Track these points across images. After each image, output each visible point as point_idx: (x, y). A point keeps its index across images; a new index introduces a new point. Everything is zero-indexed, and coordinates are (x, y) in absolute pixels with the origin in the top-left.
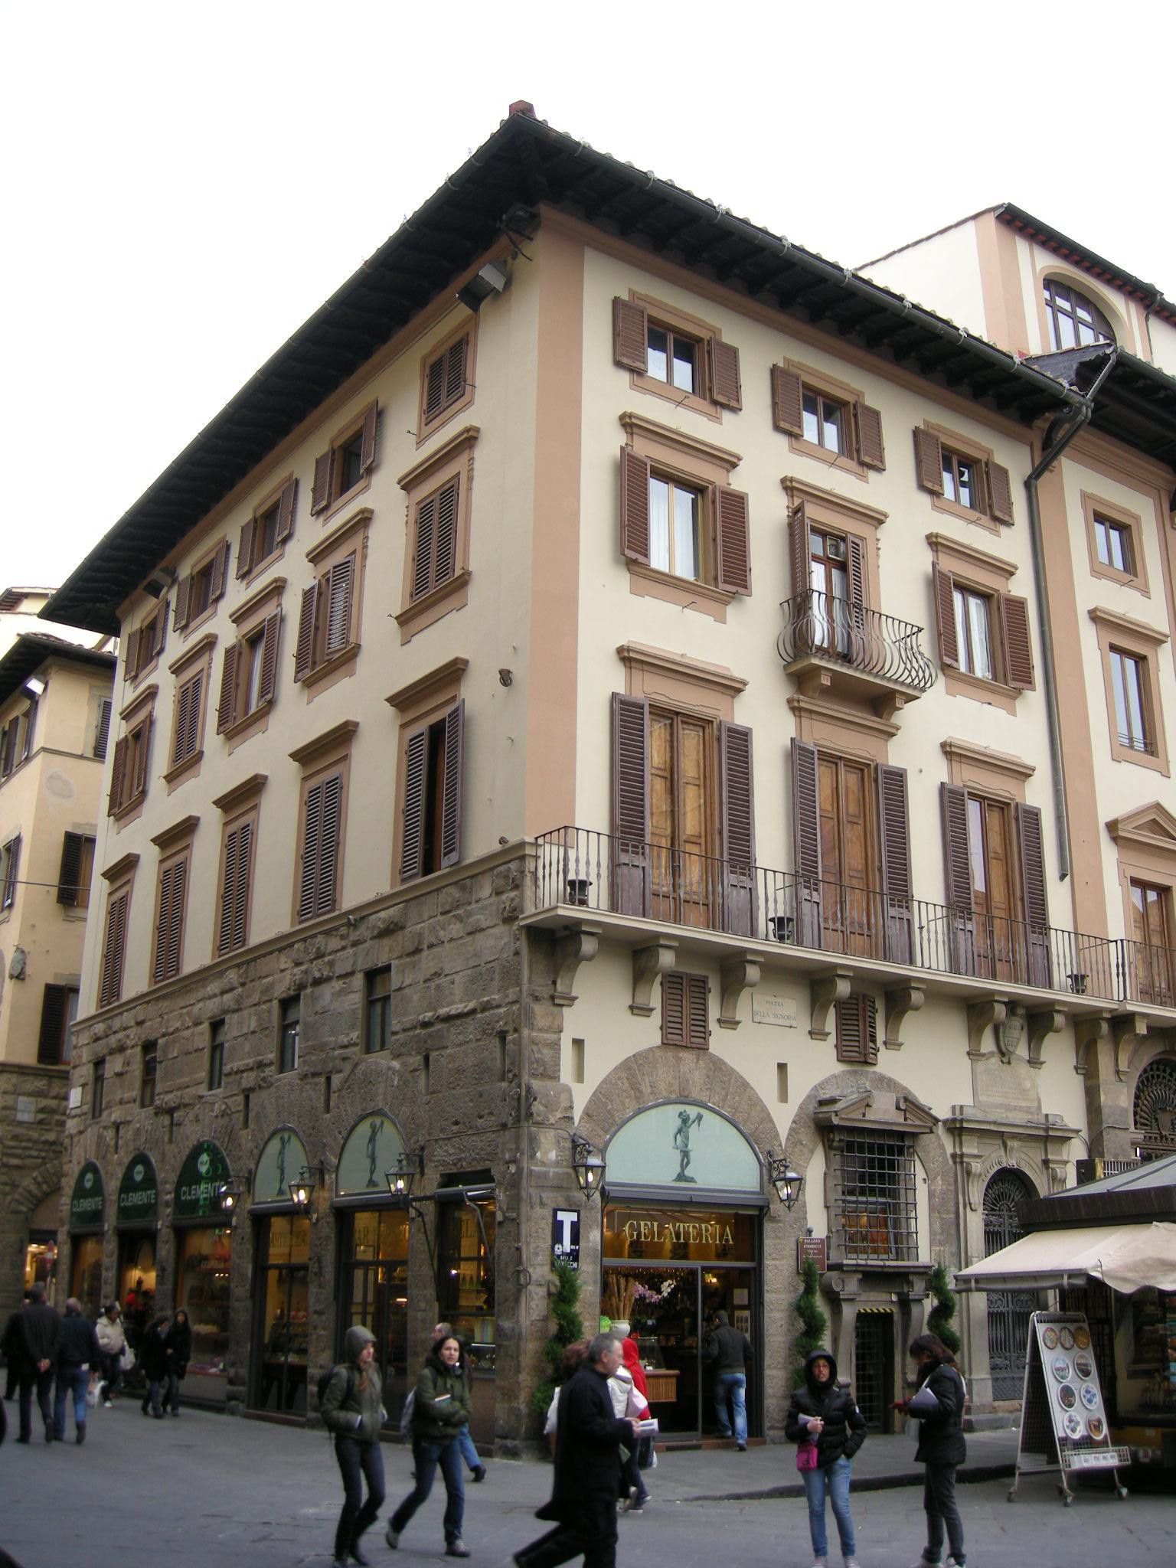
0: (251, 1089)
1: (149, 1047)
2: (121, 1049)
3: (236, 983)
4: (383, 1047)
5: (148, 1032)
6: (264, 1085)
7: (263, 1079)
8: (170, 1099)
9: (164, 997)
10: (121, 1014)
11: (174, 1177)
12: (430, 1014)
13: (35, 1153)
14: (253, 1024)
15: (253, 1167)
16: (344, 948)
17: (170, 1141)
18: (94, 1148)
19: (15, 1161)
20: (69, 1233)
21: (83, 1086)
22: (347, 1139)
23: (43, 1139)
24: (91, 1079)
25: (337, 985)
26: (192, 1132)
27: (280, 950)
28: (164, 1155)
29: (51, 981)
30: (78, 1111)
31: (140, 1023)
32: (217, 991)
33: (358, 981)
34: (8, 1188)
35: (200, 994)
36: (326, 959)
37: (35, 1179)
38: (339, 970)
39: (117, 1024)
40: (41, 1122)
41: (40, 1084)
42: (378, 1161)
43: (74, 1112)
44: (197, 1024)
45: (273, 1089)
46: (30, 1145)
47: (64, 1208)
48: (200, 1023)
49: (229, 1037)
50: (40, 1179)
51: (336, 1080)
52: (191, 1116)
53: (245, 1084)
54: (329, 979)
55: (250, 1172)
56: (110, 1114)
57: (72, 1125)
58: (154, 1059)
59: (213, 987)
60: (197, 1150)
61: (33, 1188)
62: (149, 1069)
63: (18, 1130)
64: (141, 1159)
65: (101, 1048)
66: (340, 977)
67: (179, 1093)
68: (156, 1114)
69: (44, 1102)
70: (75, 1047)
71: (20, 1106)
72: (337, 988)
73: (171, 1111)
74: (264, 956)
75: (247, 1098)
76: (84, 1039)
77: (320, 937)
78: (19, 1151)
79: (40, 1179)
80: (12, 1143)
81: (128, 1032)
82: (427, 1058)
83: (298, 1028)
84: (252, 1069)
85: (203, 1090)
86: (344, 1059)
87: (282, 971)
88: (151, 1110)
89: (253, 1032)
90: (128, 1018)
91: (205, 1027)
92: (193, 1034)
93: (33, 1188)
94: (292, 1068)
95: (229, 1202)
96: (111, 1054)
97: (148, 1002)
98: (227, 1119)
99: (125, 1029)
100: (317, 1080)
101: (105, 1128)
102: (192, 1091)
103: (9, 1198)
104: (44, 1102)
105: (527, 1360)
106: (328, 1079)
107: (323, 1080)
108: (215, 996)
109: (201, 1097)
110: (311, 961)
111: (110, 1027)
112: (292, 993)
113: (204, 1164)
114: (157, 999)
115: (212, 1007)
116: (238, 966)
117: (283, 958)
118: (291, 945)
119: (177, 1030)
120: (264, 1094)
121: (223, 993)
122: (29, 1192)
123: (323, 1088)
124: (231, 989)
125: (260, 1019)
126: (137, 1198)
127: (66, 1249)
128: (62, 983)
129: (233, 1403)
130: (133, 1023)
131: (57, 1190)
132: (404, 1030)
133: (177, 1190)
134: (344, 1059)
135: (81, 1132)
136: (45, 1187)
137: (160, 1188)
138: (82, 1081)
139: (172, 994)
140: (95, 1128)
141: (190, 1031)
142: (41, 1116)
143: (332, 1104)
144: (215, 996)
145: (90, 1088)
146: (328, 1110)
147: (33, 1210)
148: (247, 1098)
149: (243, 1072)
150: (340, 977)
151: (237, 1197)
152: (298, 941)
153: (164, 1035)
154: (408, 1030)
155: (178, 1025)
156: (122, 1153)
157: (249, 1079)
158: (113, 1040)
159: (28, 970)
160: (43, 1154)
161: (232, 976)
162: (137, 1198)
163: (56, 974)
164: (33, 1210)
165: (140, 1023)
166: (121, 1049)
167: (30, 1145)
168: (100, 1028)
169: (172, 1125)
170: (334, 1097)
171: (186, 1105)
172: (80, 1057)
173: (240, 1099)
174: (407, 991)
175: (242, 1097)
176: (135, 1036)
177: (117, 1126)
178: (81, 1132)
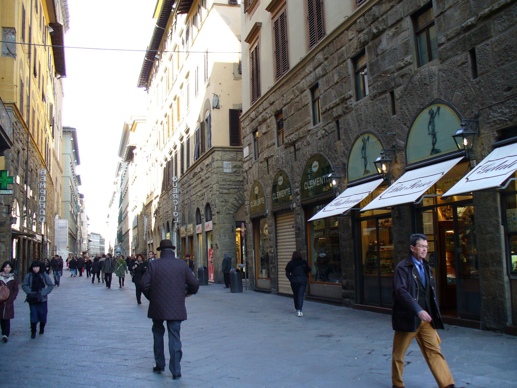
0: (340, 116)
1: (278, 114)
2: (264, 120)
3: (322, 60)
4: (431, 59)
5: (277, 106)
6: (347, 110)
7: (347, 108)
8: (293, 137)
9: (283, 85)
10: (262, 103)
11: (298, 179)
12: (472, 19)
13: (234, 187)
14: (336, 78)
15: (345, 161)
16: (392, 7)
17: (296, 160)
18: (257, 174)
19: (225, 191)
20: (250, 218)
21: (249, 145)
22: (410, 128)
23: (237, 180)
24: (252, 141)
25: (390, 32)
26: (307, 151)
27: (347, 29)
28: (292, 168)
29: (232, 108)
30: (248, 158)
31: (271, 104)
32: (312, 69)
33: (408, 23)
34: (224, 203)
35: (303, 74)
36: (380, 19)
37: (235, 198)
38: (390, 22)
39: (261, 109)
40: (235, 172)
41: (233, 154)
42: (438, 135)
43: (246, 159)
44: (302, 92)
45: (353, 112)
46: (231, 183)
47: (247, 206)
48: (305, 90)
49: (322, 92)
50: (237, 198)
51: (398, 92)
52: (305, 143)
53: (335, 115)
54: (384, 31)
55: (344, 165)
56: (263, 155)
57: (246, 166)
58: (282, 120)
59: (309, 68)
60: (313, 158)
61: (235, 202)
62: (280, 126)
63: (225, 177)
64: (281, 172)
65: (254, 124)
66: (392, 26)
67: (297, 133)
68: (286, 148)
69: (235, 163)
70: (243, 128)
71: (225, 166)
72: (391, 34)
73: (293, 144)
74: (338, 37)
75: (337, 122)
76: (246, 122)
77: (374, 8)
78: (227, 186)
79: (237, 198)
80: (223, 183)
81: (267, 110)
82: (473, 52)
83: (366, 70)
84: (338, 104)
85: (311, 127)
86: (402, 76)
87: (350, 40)
88: (283, 146)
89: (337, 83)
90: (266, 104)
91: (308, 92)
92: (301, 99)
93: (235, 202)
94: (365, 95)
95: (334, 182)
96: (260, 125)
97: (275, 92)
98: (326, 138)
99: (265, 110)
100: (383, 96)
101: (261, 162)
102: (305, 129)
103: (225, 208)
104: (235, 163)
105: (345, 291)
106: (392, 94)
107: (388, 95)
108: (311, 72)
109: (309, 131)
110: (370, 25)
111: (258, 112)
112: (359, 50)
113: (315, 167)
114: (279, 88)
115: (310, 79)
116: (322, 50)
117: (350, 33)
118: (355, 22)
119: (292, 99)
120: (349, 117)
121: (315, 69)
122: (233, 204)
123: (389, 100)
124: (320, 65)
125: (339, 73)
126: (280, 194)
127: (250, 226)
128: (237, 108)
129: (347, 300)
130: (269, 105)
131: (244, 201)
132: (449, 40)
133: (302, 184)
134: (402, 76)
135: (250, 168)
136: (240, 202)
137: (292, 186)
138: (248, 143)
139: (286, 82)
140: (257, 164)
141: (299, 97)
142: (234, 170)
143: (397, 108)
144: (311, 72)
145: (252, 145)
146: (394, 113)
147: (236, 212)
148: (337, 122)
149: (333, 108)
150: (392, 26)
151: (338, 179)
152: (359, 18)
153: (285, 105)
154: (452, 38)
155: (292, 97)
156: (271, 173)
157: (339, 110)
158: (260, 118)
159: (221, 104)
160: (238, 187)
161: (320, 57)
162: (280, 194)
163: (233, 105)
164: (236, 212)
165: (271, 104)
166: (264, 120)
167: (231, 183)
168: (253, 114)
169: (295, 150)
170: (397, 103)
171: (301, 138)
172: (246, 132)
173: (334, 124)
174: (448, 12)
175: (334, 123)
176: (271, 111)
177: (267, 160)
178: (250, 168)
